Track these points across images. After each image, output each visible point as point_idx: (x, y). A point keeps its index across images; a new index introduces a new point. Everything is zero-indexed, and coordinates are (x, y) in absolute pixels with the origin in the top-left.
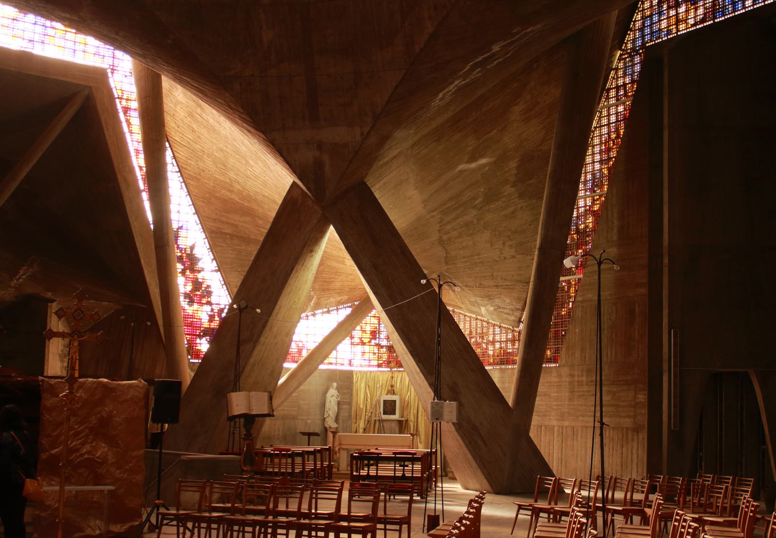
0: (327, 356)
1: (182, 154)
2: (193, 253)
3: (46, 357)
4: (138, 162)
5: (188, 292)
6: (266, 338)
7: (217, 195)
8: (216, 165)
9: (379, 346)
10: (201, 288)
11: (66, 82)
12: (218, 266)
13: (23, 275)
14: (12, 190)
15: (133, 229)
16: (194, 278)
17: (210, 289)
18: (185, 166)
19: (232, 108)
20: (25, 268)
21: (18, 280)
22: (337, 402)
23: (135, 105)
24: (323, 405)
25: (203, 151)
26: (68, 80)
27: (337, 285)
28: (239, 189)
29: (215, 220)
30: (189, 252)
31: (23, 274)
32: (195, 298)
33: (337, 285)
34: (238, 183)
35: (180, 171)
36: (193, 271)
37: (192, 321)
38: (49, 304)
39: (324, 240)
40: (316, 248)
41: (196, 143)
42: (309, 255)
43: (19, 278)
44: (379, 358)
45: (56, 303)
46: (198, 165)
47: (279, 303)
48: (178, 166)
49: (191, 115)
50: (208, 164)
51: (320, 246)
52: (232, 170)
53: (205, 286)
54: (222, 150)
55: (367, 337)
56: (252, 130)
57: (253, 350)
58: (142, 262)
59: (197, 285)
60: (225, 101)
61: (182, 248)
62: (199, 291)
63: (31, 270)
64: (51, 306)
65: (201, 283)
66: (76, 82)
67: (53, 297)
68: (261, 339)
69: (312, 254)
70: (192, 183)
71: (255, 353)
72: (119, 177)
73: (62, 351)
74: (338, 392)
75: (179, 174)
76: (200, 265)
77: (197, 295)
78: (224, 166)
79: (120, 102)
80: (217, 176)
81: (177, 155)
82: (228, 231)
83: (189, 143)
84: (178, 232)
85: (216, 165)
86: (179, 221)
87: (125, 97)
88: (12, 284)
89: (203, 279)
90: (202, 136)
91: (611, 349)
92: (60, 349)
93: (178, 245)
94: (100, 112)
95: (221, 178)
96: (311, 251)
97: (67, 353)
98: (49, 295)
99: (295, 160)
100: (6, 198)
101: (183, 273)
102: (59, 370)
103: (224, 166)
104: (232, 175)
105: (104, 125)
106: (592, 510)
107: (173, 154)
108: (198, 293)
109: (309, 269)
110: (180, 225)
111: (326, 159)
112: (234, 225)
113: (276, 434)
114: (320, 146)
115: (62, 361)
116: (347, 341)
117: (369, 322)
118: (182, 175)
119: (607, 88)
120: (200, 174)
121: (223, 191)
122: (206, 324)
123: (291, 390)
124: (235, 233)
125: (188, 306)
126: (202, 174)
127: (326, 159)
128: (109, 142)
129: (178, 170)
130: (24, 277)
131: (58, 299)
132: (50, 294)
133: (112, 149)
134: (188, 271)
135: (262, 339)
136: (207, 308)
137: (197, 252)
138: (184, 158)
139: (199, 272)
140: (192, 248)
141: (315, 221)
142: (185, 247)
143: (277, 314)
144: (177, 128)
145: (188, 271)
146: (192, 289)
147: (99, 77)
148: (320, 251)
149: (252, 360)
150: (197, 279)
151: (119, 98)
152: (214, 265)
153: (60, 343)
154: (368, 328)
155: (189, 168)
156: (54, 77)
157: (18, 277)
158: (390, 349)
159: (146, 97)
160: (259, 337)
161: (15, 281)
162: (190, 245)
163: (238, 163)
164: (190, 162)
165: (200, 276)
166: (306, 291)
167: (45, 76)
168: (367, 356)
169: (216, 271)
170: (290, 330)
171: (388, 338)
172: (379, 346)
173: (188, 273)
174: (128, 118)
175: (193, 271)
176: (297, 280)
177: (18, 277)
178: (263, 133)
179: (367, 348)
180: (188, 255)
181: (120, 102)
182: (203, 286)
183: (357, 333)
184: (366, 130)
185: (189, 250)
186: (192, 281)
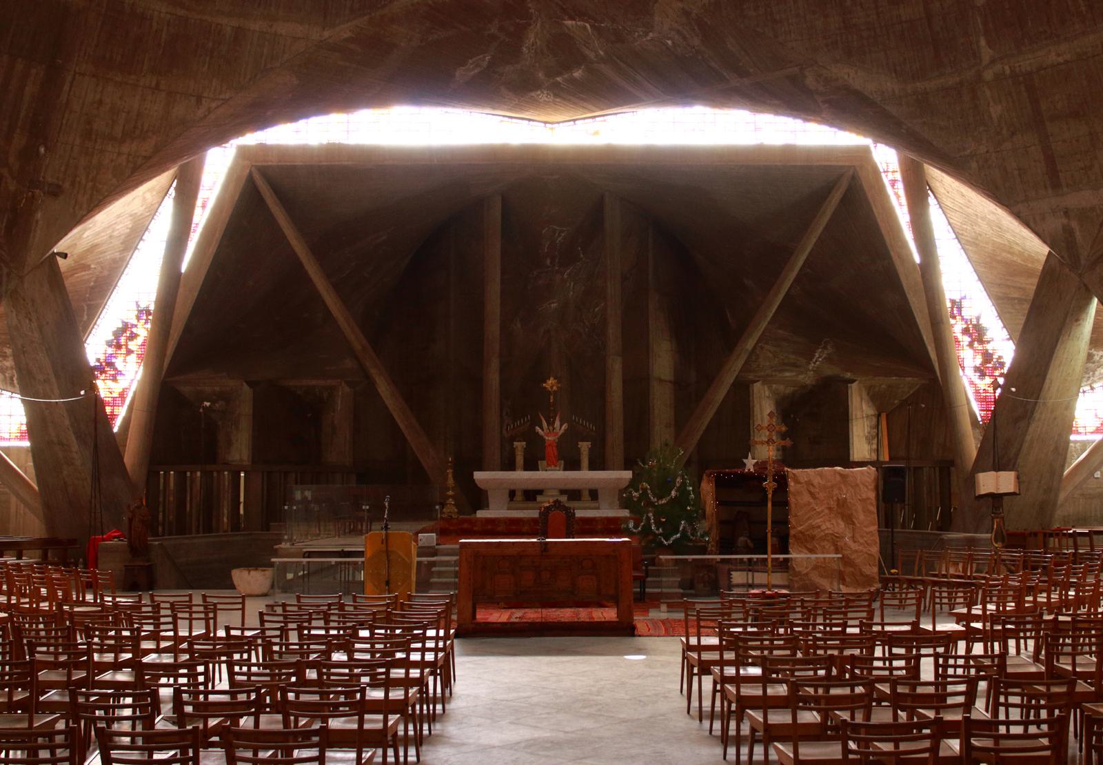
2: (980, 322)
3: (851, 441)
5: (978, 365)
6: (1041, 413)
7: (999, 258)
8: (992, 228)
10: (992, 360)
11: (831, 166)
12: (1009, 335)
13: (819, 358)
14: (778, 304)
15: (912, 305)
16: (983, 350)
17: (1002, 360)
18: (961, 232)
19: (974, 185)
20: (820, 350)
21: (815, 363)
23: (898, 176)
25: (977, 215)
26: (833, 163)
28: (1020, 251)
29: (999, 285)
30: (975, 323)
31: (819, 356)
32: (987, 371)
34: (1017, 244)
35: (957, 238)
36: (981, 342)
37: (986, 396)
38: (849, 385)
39: (1091, 306)
40: (1084, 316)
41: (968, 208)
42: (1075, 324)
43: (816, 361)
45: (857, 382)
46: (973, 229)
47: (1048, 377)
48: (954, 232)
51: (1087, 313)
52: (1008, 232)
53: (997, 357)
54: (993, 213)
56: (998, 204)
57: (1028, 427)
58: (925, 338)
60: (966, 179)
61: (967, 319)
62: (990, 363)
63: (826, 352)
64: (851, 387)
65: (991, 355)
66: (840, 164)
67: (853, 377)
68: (1035, 415)
69: (1079, 323)
70: (970, 248)
71: (1031, 429)
72: (892, 254)
73: (869, 433)
75: (956, 240)
76: (988, 336)
77: (988, 367)
78: (1000, 228)
79: (887, 176)
80: (995, 239)
81: (951, 221)
82: (1016, 295)
83: (961, 208)
84: (961, 302)
85: (992, 228)
86: (961, 291)
87: (890, 170)
88: (811, 368)
89: (993, 350)
90: (971, 200)
91: (181, 504)
92: (866, 431)
93: (962, 317)
94: (866, 189)
95: (998, 240)
96: (1077, 320)
97: (875, 434)
98: (848, 375)
99: (1044, 230)
100: (774, 311)
101: (971, 345)
102: (867, 454)
103: (1000, 228)
104: (1008, 236)
105: (872, 203)
107: (948, 220)
108: (990, 365)
109: (1078, 339)
110: (963, 295)
111: (1074, 224)
112: (1020, 288)
113: (1093, 515)
114: (1066, 213)
115: (870, 443)
118: (959, 242)
120: (977, 239)
121: (1004, 254)
123: (1094, 466)
124: (1024, 297)
125: (979, 380)
126: (979, 238)
127: (1074, 224)
128: (879, 220)
129: (955, 237)
130: (820, 359)
131: (859, 379)
132: (849, 374)
133: (882, 225)
134: (976, 343)
135: (1037, 415)
137: (984, 322)
138: (959, 224)
139: (988, 342)
140: (978, 319)
141: (1074, 290)
142: (970, 318)
143: (1049, 388)
144: (947, 194)
145: (976, 343)
146: (982, 362)
148: (1088, 318)
149: (1028, 438)
150: (987, 350)
151: (885, 172)
153: (866, 424)
155: (965, 234)
156: (818, 164)
157: (814, 360)
159: (907, 170)
160: (1032, 413)
161: (813, 365)
162: (977, 315)
163: (1011, 225)
164: (965, 226)
165: (989, 347)
166: (1081, 361)
167: (809, 164)
169: (1008, 339)
170: (1069, 403)
173: (976, 344)
174: (896, 190)
175: (981, 342)
176: (1066, 351)
177: (814, 360)
178: (1007, 206)
180: (975, 326)
181: (887, 176)
182: (994, 357)
185: (975, 320)
186: (982, 353)
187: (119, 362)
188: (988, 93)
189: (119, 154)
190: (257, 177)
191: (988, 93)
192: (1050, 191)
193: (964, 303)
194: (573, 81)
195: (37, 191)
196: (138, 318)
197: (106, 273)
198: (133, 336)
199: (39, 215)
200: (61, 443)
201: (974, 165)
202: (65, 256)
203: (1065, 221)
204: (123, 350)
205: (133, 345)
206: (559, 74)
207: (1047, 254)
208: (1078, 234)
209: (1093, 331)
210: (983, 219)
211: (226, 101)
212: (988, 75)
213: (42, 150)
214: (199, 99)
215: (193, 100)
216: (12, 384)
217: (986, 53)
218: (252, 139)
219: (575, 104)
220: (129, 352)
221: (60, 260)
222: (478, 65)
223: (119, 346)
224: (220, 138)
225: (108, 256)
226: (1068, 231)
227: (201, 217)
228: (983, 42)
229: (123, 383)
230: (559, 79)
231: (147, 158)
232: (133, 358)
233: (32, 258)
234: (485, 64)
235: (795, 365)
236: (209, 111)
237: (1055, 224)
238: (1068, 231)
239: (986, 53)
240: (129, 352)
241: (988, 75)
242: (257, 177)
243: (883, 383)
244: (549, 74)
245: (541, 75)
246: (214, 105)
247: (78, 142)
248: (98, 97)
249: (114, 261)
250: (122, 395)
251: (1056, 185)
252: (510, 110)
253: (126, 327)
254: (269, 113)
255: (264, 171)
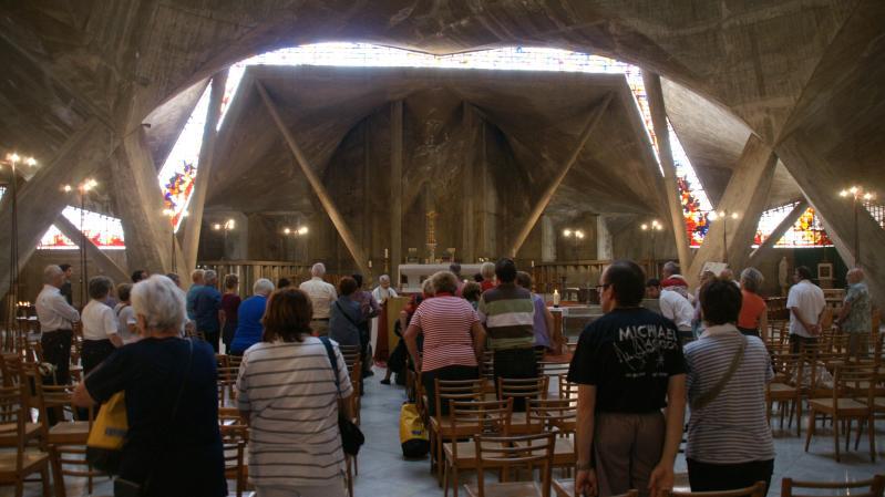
0: (778, 240)
1: (674, 119)
4: (649, 127)
9: (815, 231)
22: (722, 201)
24: (777, 271)
27: (782, 192)
33: (782, 192)
36: (687, 191)
44: (815, 239)
49: (679, 95)
50: (692, 124)
55: (805, 225)
59: (690, 200)
74: (856, 333)
76: (691, 187)
104: (708, 129)
106: (820, 265)
111: (772, 118)
114: (768, 111)
116: (792, 228)
117: (807, 215)
119: (621, 339)
122: (698, 224)
127: (772, 118)
136: (697, 214)
147: (620, 80)
152: (700, 187)
154: (806, 220)
158: (823, 233)
165: (692, 194)
168: (806, 238)
171: (821, 225)
172: (815, 231)
179: (805, 233)
183: (798, 223)
184: (798, 97)
187: (173, 198)
188: (724, 37)
189: (186, 60)
190: (260, 88)
191: (724, 37)
192: (758, 97)
193: (188, 163)
194: (459, 27)
195: (134, 83)
196: (186, 170)
197: (165, 142)
198: (182, 182)
199: (134, 98)
200: (145, 246)
201: (712, 81)
202: (149, 126)
203: (766, 115)
204: (176, 191)
205: (183, 187)
206: (453, 22)
207: (748, 137)
208: (774, 124)
209: (728, 181)
210: (692, 118)
211: (253, 29)
212: (725, 26)
213: (137, 55)
214: (237, 26)
215: (233, 27)
216: (107, 211)
217: (725, 12)
218: (255, 60)
219: (458, 42)
220: (180, 192)
221: (146, 128)
222: (405, 14)
223: (173, 188)
224: (208, 65)
225: (167, 132)
226: (768, 122)
227: (225, 109)
228: (724, 5)
229: (177, 210)
230: (452, 25)
231: (203, 64)
232: (182, 196)
233: (130, 126)
234: (409, 14)
235: (567, 205)
236: (243, 35)
237: (760, 117)
238: (768, 122)
239: (725, 12)
240: (180, 192)
241: (725, 26)
242: (260, 88)
243: (615, 216)
244: (447, 22)
245: (441, 22)
246: (245, 31)
247: (160, 50)
248: (174, 21)
249: (170, 135)
250: (176, 218)
251: (762, 94)
252: (417, 46)
253: (178, 176)
254: (278, 39)
255: (263, 83)
